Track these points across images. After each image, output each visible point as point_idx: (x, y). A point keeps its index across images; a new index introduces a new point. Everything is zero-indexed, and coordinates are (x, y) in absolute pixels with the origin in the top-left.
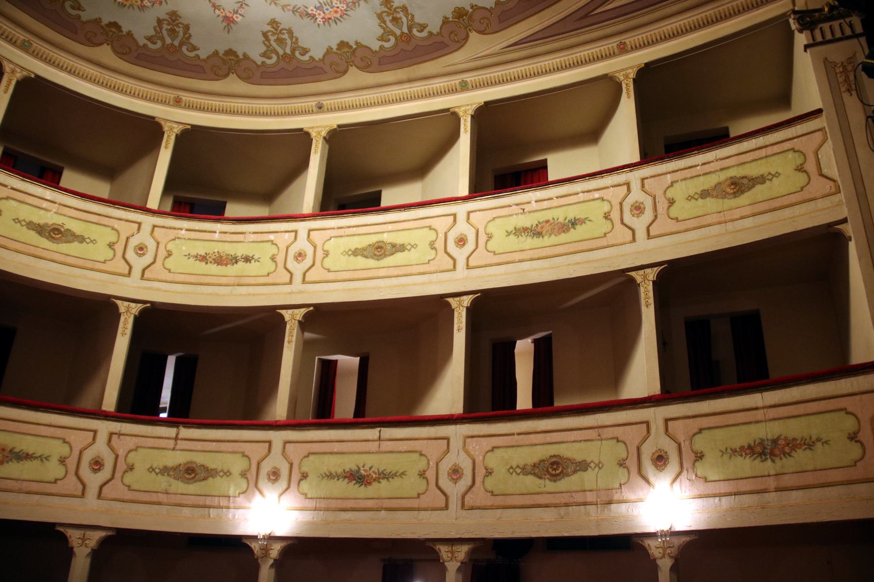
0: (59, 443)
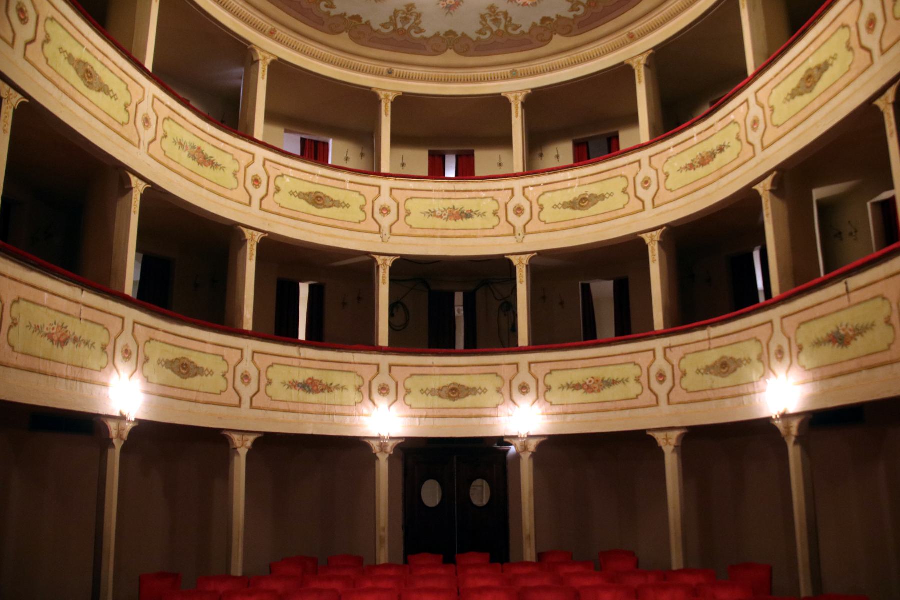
0: (632, 366)
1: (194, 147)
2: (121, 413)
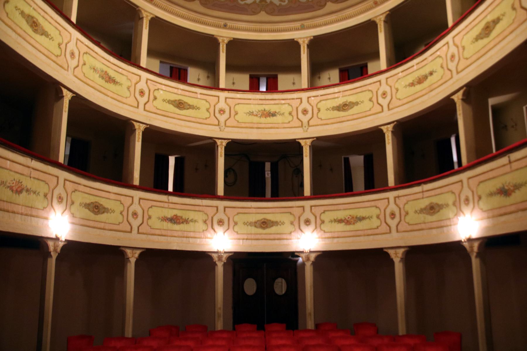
0: (374, 208)
1: (102, 71)
2: (56, 236)
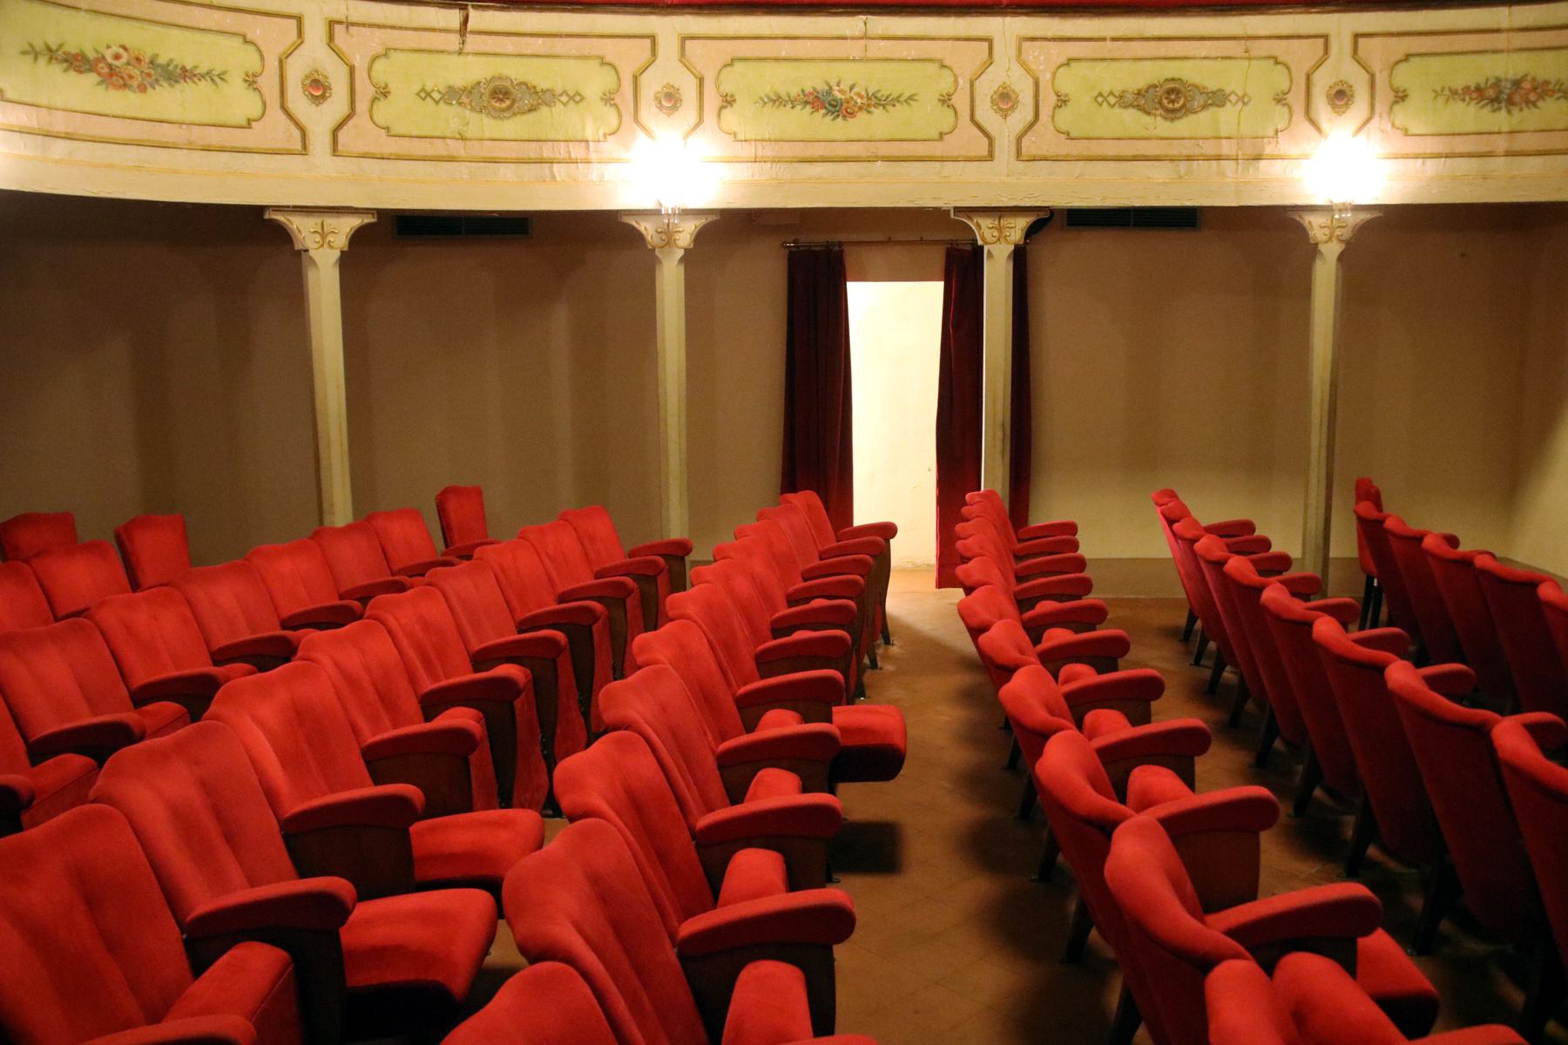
0: (236, 43)
